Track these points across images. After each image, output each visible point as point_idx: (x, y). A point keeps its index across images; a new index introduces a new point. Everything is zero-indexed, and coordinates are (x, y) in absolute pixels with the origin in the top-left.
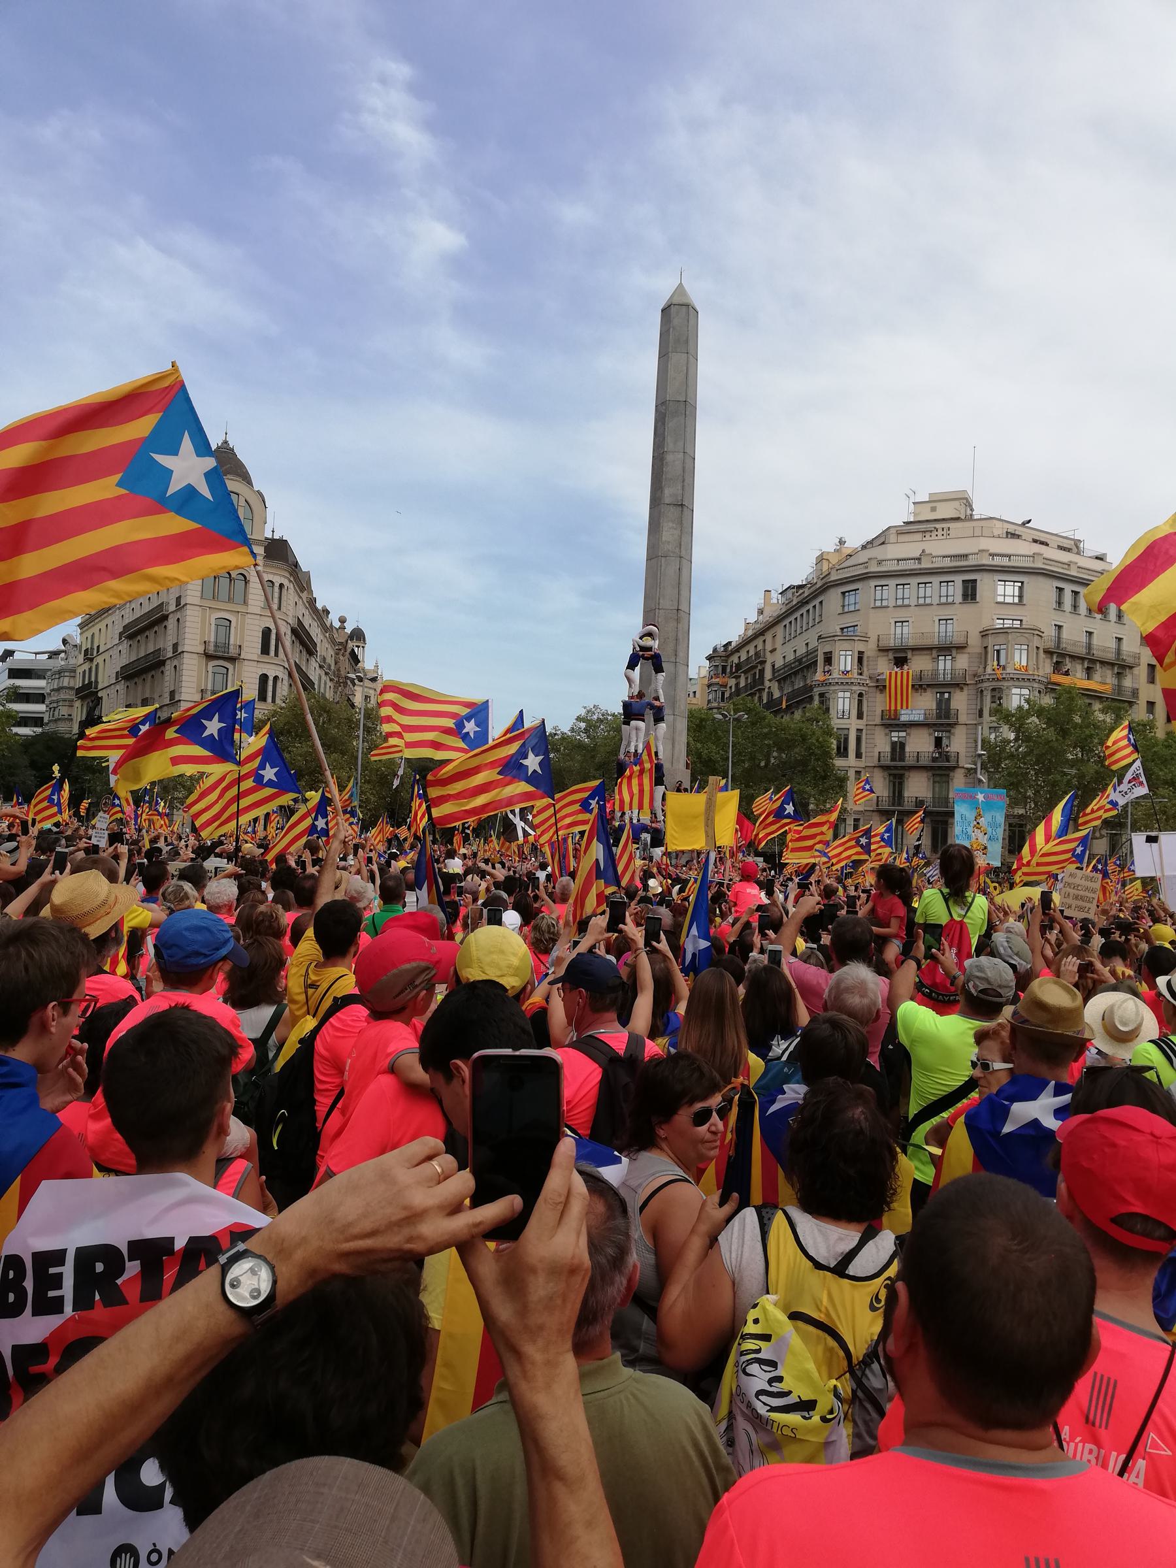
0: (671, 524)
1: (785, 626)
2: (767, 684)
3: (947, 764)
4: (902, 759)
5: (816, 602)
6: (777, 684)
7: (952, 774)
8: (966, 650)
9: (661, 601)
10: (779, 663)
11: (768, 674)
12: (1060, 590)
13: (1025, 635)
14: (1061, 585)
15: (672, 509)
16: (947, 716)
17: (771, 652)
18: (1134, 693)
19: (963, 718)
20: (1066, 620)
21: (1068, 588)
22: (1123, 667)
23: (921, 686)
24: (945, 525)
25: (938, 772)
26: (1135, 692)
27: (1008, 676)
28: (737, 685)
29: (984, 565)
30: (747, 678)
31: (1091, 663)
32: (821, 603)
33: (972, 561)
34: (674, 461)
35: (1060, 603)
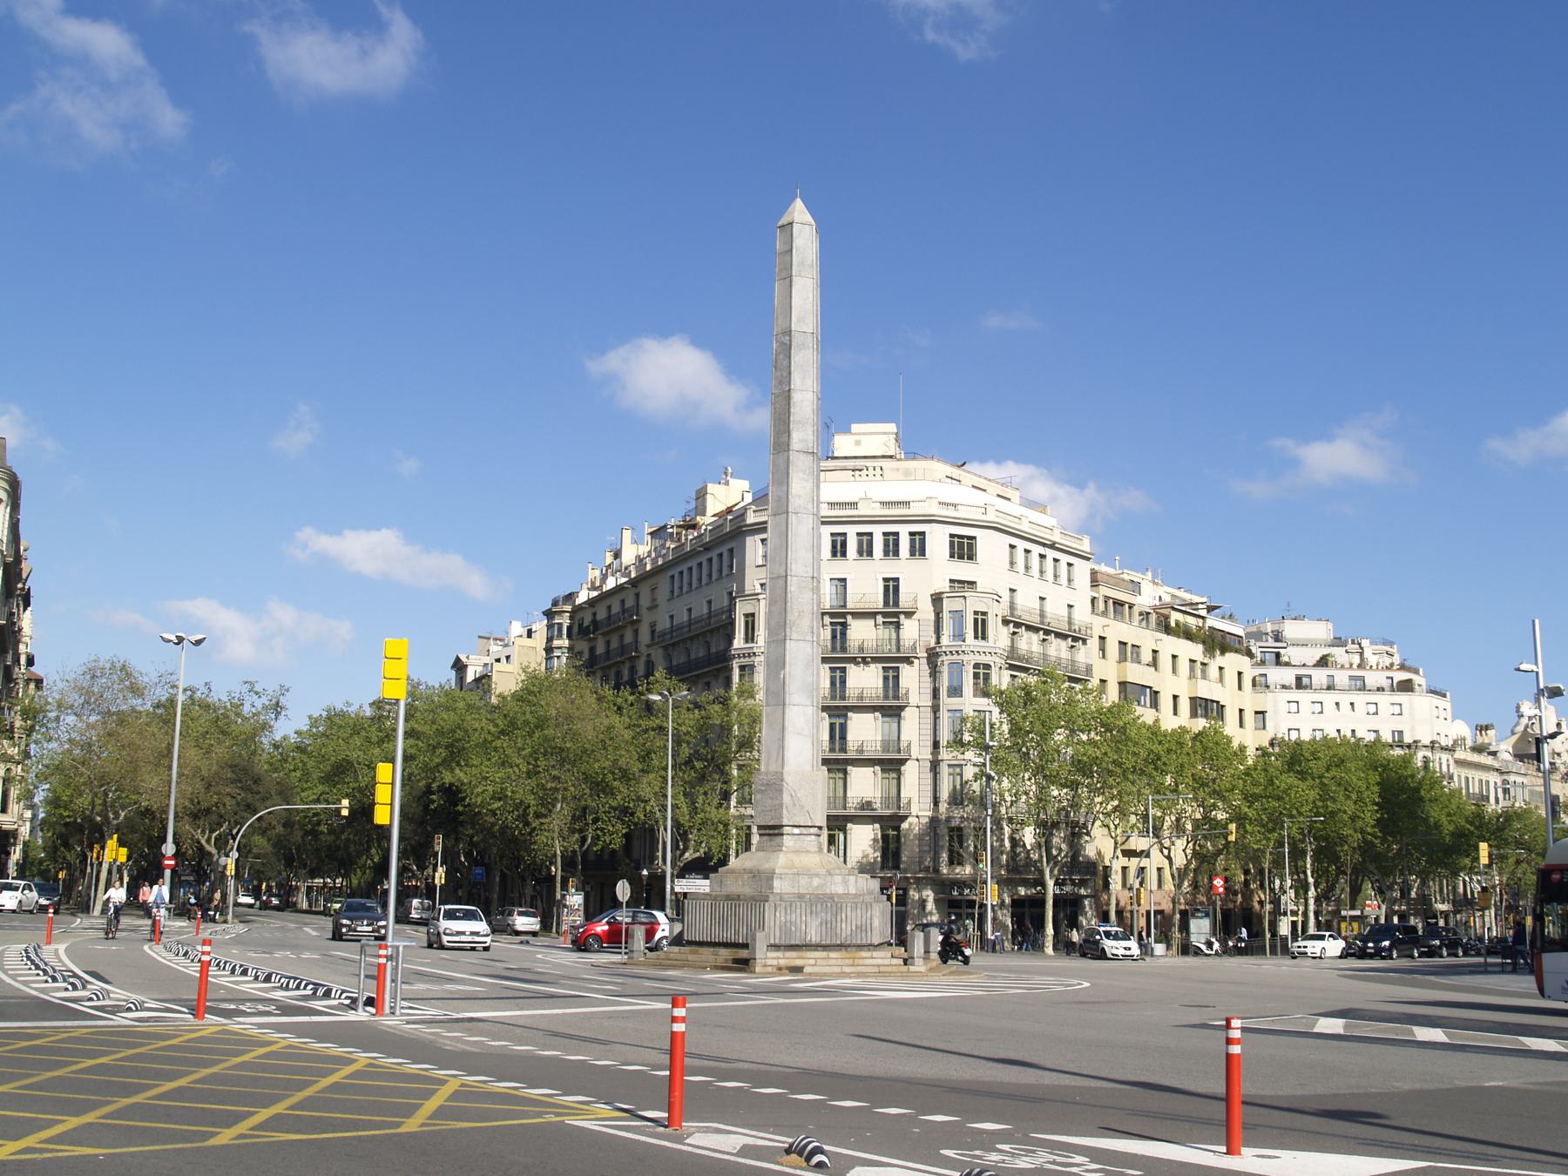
0: (801, 475)
1: (673, 577)
2: (643, 649)
3: (842, 756)
4: (844, 750)
5: (724, 549)
6: (661, 651)
7: (903, 768)
8: (915, 616)
9: (793, 566)
10: (664, 624)
11: (645, 637)
12: (1012, 547)
13: (985, 600)
14: (1014, 541)
15: (802, 456)
16: (896, 697)
17: (649, 609)
18: (1087, 670)
19: (914, 699)
20: (1018, 581)
21: (1022, 545)
22: (1075, 639)
23: (864, 658)
24: (878, 463)
25: (834, 767)
26: (1089, 669)
27: (968, 648)
28: (592, 650)
29: (933, 516)
30: (608, 643)
31: (1046, 631)
32: (731, 551)
33: (915, 510)
34: (802, 401)
35: (1012, 563)
